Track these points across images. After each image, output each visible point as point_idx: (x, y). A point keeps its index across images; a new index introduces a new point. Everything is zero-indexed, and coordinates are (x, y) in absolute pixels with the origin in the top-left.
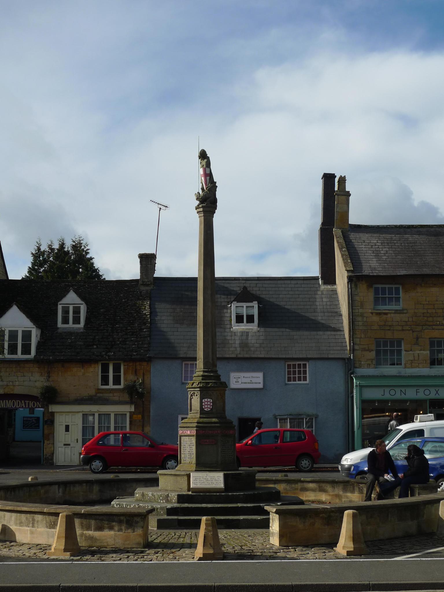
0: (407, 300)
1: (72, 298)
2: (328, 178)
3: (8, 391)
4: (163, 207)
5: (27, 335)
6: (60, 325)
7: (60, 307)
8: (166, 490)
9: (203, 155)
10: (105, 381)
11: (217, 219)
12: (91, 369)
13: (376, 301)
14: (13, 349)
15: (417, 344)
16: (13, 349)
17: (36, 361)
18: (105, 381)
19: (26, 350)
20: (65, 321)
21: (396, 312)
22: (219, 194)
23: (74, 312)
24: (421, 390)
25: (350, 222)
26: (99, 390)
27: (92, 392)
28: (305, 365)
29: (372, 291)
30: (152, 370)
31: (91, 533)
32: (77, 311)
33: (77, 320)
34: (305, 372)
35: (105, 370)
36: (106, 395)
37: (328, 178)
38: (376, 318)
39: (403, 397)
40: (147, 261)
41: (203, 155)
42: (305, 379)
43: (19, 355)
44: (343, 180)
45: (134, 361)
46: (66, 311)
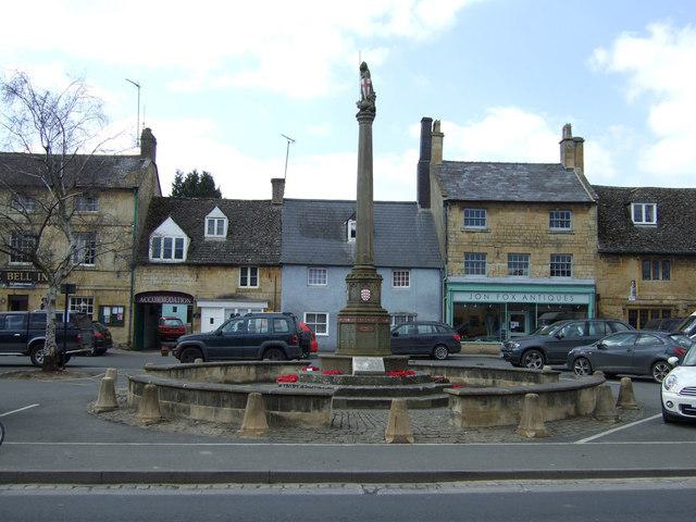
0: (493, 220)
1: (216, 213)
2: (426, 122)
3: (162, 289)
4: (291, 141)
5: (180, 242)
6: (206, 235)
7: (207, 220)
8: (207, 366)
9: (364, 68)
10: (244, 283)
11: (376, 125)
12: (232, 272)
13: (466, 223)
14: (167, 255)
15: (498, 257)
16: (167, 255)
17: (187, 265)
18: (244, 283)
19: (179, 254)
20: (156, 255)
21: (482, 231)
22: (378, 104)
23: (177, 244)
24: (501, 295)
25: (443, 159)
26: (238, 290)
27: (234, 291)
28: (407, 273)
29: (463, 214)
30: (283, 274)
31: (277, 413)
32: (221, 222)
33: (220, 231)
34: (407, 279)
35: (244, 273)
36: (244, 294)
37: (426, 122)
38: (465, 236)
39: (487, 300)
40: (278, 184)
41: (364, 68)
42: (407, 284)
43: (173, 260)
44: (437, 124)
45: (269, 266)
46: (211, 222)
